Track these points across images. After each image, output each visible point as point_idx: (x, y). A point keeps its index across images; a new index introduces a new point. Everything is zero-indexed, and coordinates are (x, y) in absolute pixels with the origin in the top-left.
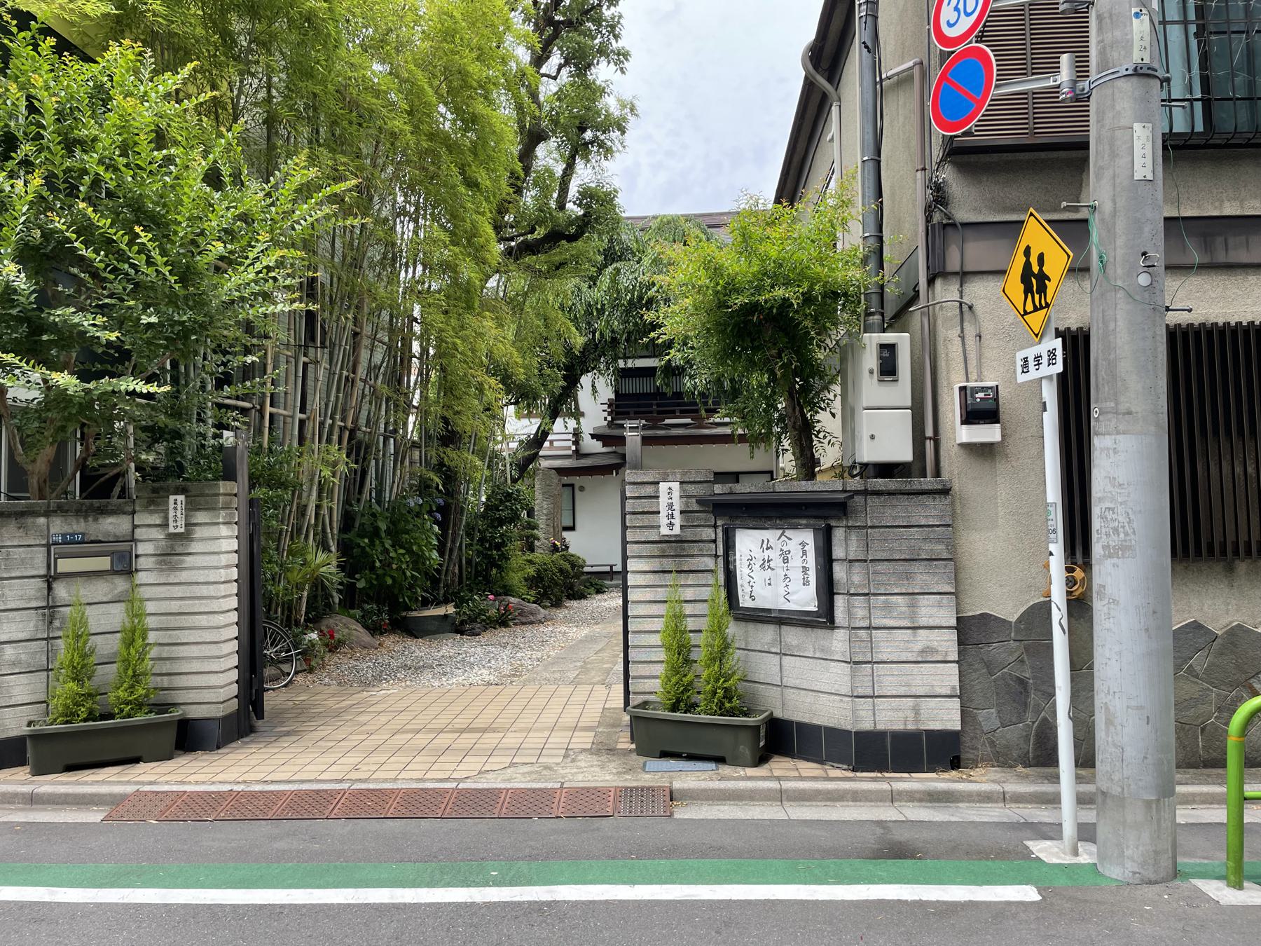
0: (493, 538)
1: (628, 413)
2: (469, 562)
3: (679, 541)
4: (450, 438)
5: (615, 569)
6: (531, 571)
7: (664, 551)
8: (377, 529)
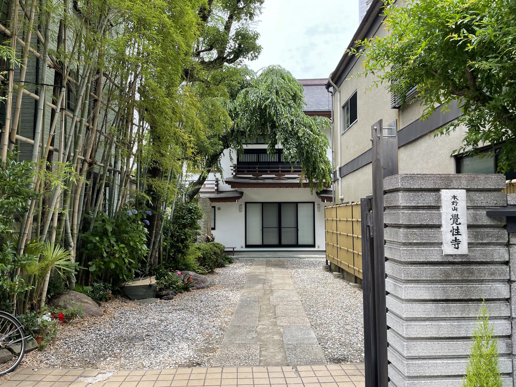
0: (180, 235)
1: (244, 171)
2: (165, 249)
3: (466, 262)
4: (155, 172)
5: (235, 250)
6: (200, 254)
7: (447, 274)
8: (106, 230)
